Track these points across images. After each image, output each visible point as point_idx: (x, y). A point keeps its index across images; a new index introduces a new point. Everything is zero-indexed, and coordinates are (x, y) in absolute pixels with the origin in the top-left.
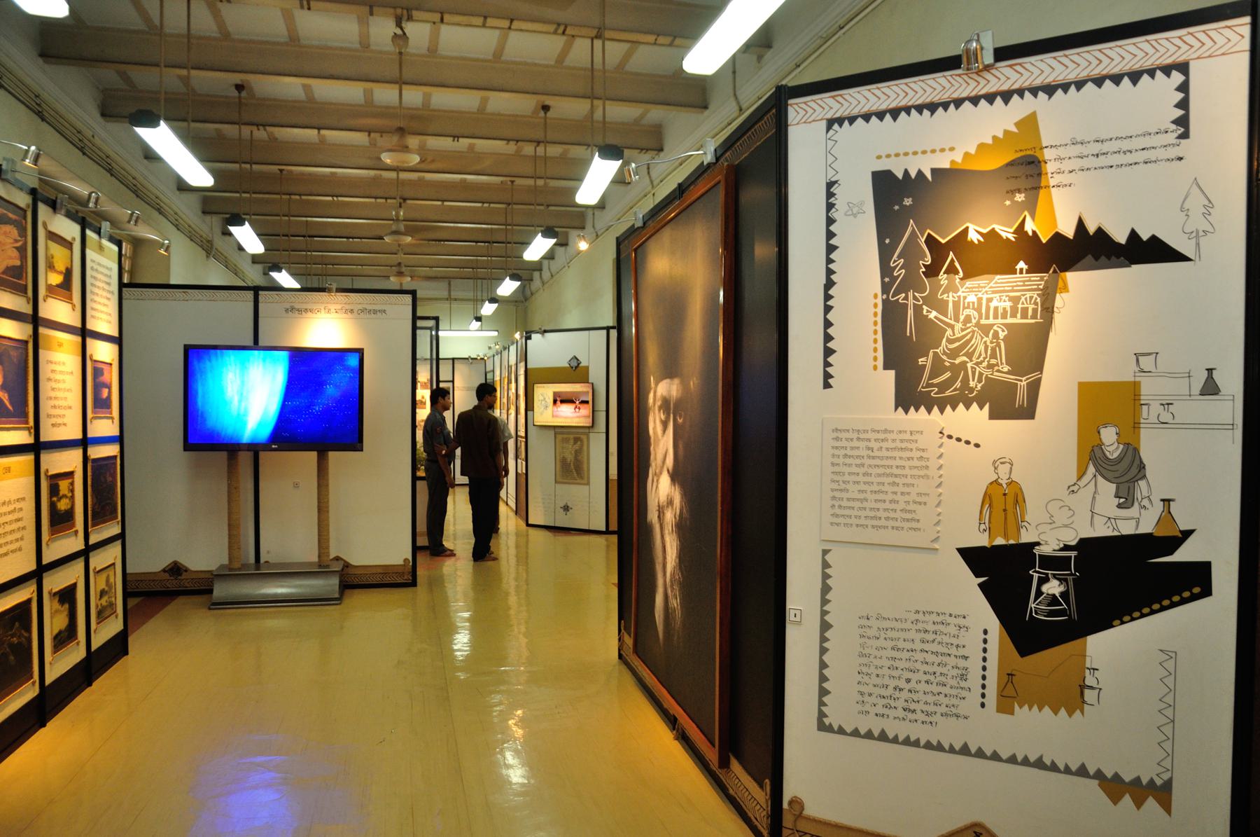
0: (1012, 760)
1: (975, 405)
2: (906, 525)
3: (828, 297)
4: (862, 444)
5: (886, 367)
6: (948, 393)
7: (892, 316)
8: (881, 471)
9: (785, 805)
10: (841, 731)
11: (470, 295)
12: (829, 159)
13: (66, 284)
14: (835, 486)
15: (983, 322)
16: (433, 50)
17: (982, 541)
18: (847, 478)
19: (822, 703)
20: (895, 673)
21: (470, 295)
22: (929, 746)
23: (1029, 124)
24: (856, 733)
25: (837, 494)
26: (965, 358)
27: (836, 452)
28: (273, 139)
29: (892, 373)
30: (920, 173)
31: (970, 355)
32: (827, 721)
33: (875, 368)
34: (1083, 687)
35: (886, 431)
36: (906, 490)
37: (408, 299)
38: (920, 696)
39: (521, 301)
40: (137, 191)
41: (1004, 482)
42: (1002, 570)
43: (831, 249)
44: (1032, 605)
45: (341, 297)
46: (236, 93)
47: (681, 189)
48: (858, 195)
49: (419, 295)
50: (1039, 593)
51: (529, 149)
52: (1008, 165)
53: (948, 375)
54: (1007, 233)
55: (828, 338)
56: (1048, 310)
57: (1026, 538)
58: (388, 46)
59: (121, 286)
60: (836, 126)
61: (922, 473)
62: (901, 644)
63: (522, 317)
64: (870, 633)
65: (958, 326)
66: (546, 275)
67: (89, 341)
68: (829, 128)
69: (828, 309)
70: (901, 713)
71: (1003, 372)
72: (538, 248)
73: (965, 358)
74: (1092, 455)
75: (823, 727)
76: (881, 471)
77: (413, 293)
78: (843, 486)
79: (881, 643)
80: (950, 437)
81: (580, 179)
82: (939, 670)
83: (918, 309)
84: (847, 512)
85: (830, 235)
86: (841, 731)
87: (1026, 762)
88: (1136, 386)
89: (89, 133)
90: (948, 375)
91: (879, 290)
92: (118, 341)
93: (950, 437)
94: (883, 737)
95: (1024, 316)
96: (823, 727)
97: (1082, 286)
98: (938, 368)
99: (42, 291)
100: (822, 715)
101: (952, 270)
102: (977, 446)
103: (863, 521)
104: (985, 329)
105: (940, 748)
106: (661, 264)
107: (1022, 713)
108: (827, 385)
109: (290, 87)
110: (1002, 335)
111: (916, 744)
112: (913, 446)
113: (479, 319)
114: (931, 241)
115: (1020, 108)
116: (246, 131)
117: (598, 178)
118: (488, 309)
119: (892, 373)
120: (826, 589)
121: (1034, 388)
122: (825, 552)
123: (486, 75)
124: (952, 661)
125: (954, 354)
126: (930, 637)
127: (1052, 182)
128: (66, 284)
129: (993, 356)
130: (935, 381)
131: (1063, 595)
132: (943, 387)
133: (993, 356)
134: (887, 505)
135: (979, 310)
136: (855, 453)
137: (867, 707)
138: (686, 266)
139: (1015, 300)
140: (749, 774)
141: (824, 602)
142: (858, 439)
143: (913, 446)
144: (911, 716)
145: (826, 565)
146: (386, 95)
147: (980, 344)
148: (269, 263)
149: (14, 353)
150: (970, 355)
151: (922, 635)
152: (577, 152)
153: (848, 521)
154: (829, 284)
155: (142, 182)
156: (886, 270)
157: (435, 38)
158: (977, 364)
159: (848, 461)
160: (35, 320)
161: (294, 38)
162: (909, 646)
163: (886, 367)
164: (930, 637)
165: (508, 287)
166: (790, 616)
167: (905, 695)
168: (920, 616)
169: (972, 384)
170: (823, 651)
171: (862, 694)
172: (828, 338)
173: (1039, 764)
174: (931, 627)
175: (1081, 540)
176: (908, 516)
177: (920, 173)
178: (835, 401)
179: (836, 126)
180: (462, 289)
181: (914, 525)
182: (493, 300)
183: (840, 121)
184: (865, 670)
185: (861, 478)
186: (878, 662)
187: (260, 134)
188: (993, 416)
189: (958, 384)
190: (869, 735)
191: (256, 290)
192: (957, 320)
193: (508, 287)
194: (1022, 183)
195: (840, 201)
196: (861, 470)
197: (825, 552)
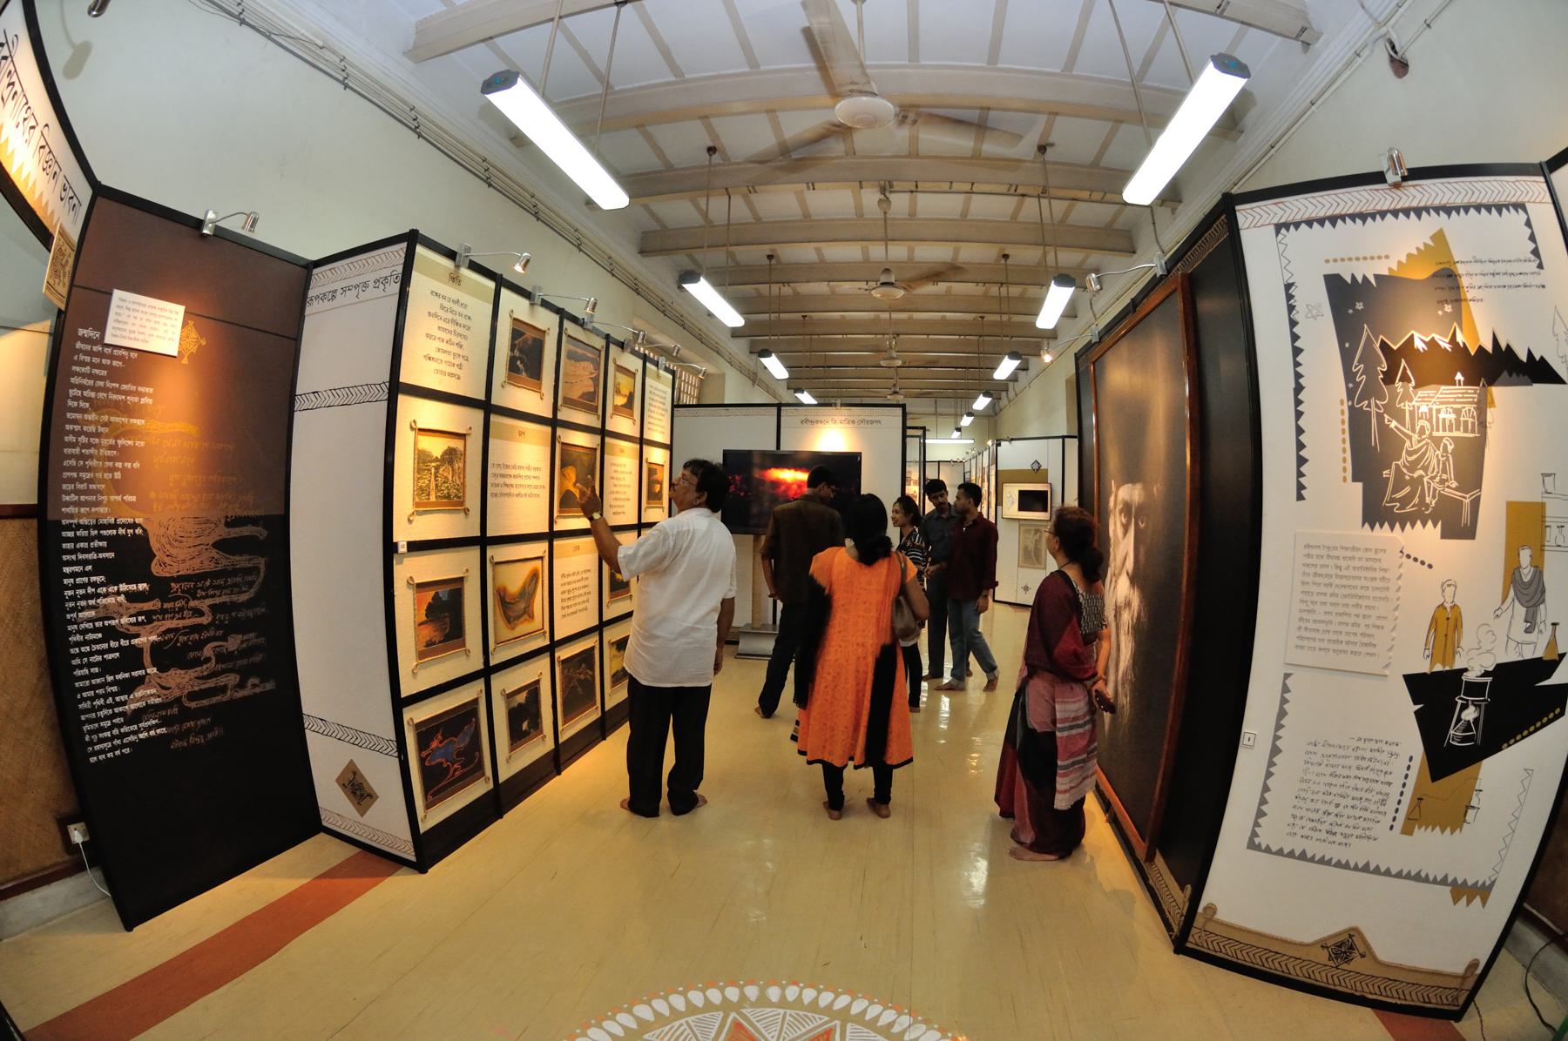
0: (1399, 875)
1: (1430, 523)
2: (1364, 650)
3: (1298, 402)
4: (1332, 562)
5: (1354, 480)
6: (1408, 509)
7: (1358, 423)
8: (1348, 591)
9: (1200, 910)
10: (1268, 850)
11: (952, 411)
12: (1283, 263)
13: (629, 404)
14: (1304, 607)
15: (1435, 434)
16: (913, 214)
17: (1423, 667)
18: (1315, 598)
19: (1256, 824)
20: (1328, 798)
21: (952, 411)
22: (1339, 865)
23: (1439, 237)
24: (1280, 852)
25: (1305, 615)
26: (1421, 472)
27: (1307, 570)
28: (796, 294)
29: (1360, 485)
30: (1365, 278)
31: (1425, 469)
32: (1257, 840)
33: (1345, 479)
34: (1469, 807)
35: (1353, 549)
36: (1367, 612)
37: (899, 411)
38: (1344, 820)
39: (992, 414)
40: (701, 338)
41: (1448, 606)
42: (1433, 693)
43: (1297, 351)
44: (1452, 732)
45: (845, 410)
46: (767, 262)
47: (1135, 304)
48: (1314, 297)
49: (908, 409)
50: (1459, 719)
51: (994, 290)
52: (1435, 275)
53: (1408, 489)
54: (1444, 343)
55: (1300, 446)
56: (1483, 424)
57: (1457, 666)
58: (878, 214)
59: (674, 406)
60: (1283, 231)
61: (1382, 595)
62: (1339, 771)
63: (992, 427)
64: (1314, 759)
65: (1415, 437)
66: (1011, 394)
67: (645, 448)
68: (1278, 232)
69: (1299, 414)
70: (1323, 835)
71: (1451, 490)
72: (1005, 369)
73: (1421, 472)
74: (1512, 576)
75: (1253, 845)
76: (1348, 591)
77: (903, 406)
78: (1311, 607)
79: (1323, 769)
80: (1408, 556)
81: (1036, 314)
82: (1365, 795)
83: (1380, 417)
84: (1312, 635)
85: (1295, 337)
86: (1268, 850)
87: (1408, 877)
88: (1543, 505)
89: (668, 300)
90: (1408, 489)
91: (1345, 397)
92: (669, 447)
93: (1408, 556)
94: (1302, 856)
95: (1466, 431)
96: (1253, 845)
97: (1506, 397)
98: (1400, 483)
99: (609, 410)
100: (1254, 834)
101: (1405, 379)
102: (1430, 566)
103: (1325, 645)
104: (1437, 441)
105: (1346, 866)
106: (1119, 376)
107: (1419, 833)
108: (1300, 497)
109: (805, 253)
110: (1450, 448)
111: (1328, 863)
112: (1376, 565)
113: (959, 429)
114: (1384, 346)
115: (1433, 222)
116: (775, 288)
117: (1056, 300)
118: (966, 421)
119: (1360, 485)
120: (1282, 714)
121: (1476, 503)
122: (1287, 676)
123: (958, 230)
124: (1377, 787)
125: (1412, 467)
126: (1364, 764)
127: (1469, 296)
128: (629, 404)
129: (1444, 471)
130: (1398, 496)
131: (1476, 720)
132: (1405, 501)
133: (1444, 471)
134: (1349, 629)
135: (1430, 421)
136: (1324, 571)
137: (1296, 830)
138: (1148, 381)
139: (1458, 412)
140: (1173, 873)
141: (1279, 727)
142: (1329, 556)
143: (1376, 565)
144: (1331, 838)
145: (1286, 689)
146: (877, 251)
147: (1433, 457)
148: (794, 385)
149: (585, 458)
150: (1425, 469)
151: (1359, 762)
152: (1032, 291)
153: (1312, 644)
154: (1299, 389)
155: (696, 325)
156: (1349, 376)
157: (913, 204)
158: (1432, 478)
159: (1318, 580)
160: (603, 432)
161: (807, 216)
162: (1345, 772)
163: (1354, 480)
164: (1364, 764)
165: (981, 403)
166: (1244, 740)
167: (1331, 819)
168: (1361, 744)
169: (1428, 500)
170: (1269, 775)
171: (1294, 817)
172: (1300, 446)
173: (1418, 878)
174: (1368, 755)
175: (1498, 666)
176: (1366, 640)
177: (1365, 278)
178: (1305, 515)
179: (1283, 231)
180: (946, 406)
181: (1371, 650)
182: (969, 414)
183: (1287, 226)
184: (1303, 794)
185: (1328, 599)
186: (1316, 788)
187: (786, 290)
188: (1444, 536)
189: (1416, 500)
190: (1291, 855)
191: (779, 406)
192: (1413, 431)
193: (981, 403)
194: (1446, 295)
195: (1298, 302)
196: (1329, 590)
197: (1287, 676)
